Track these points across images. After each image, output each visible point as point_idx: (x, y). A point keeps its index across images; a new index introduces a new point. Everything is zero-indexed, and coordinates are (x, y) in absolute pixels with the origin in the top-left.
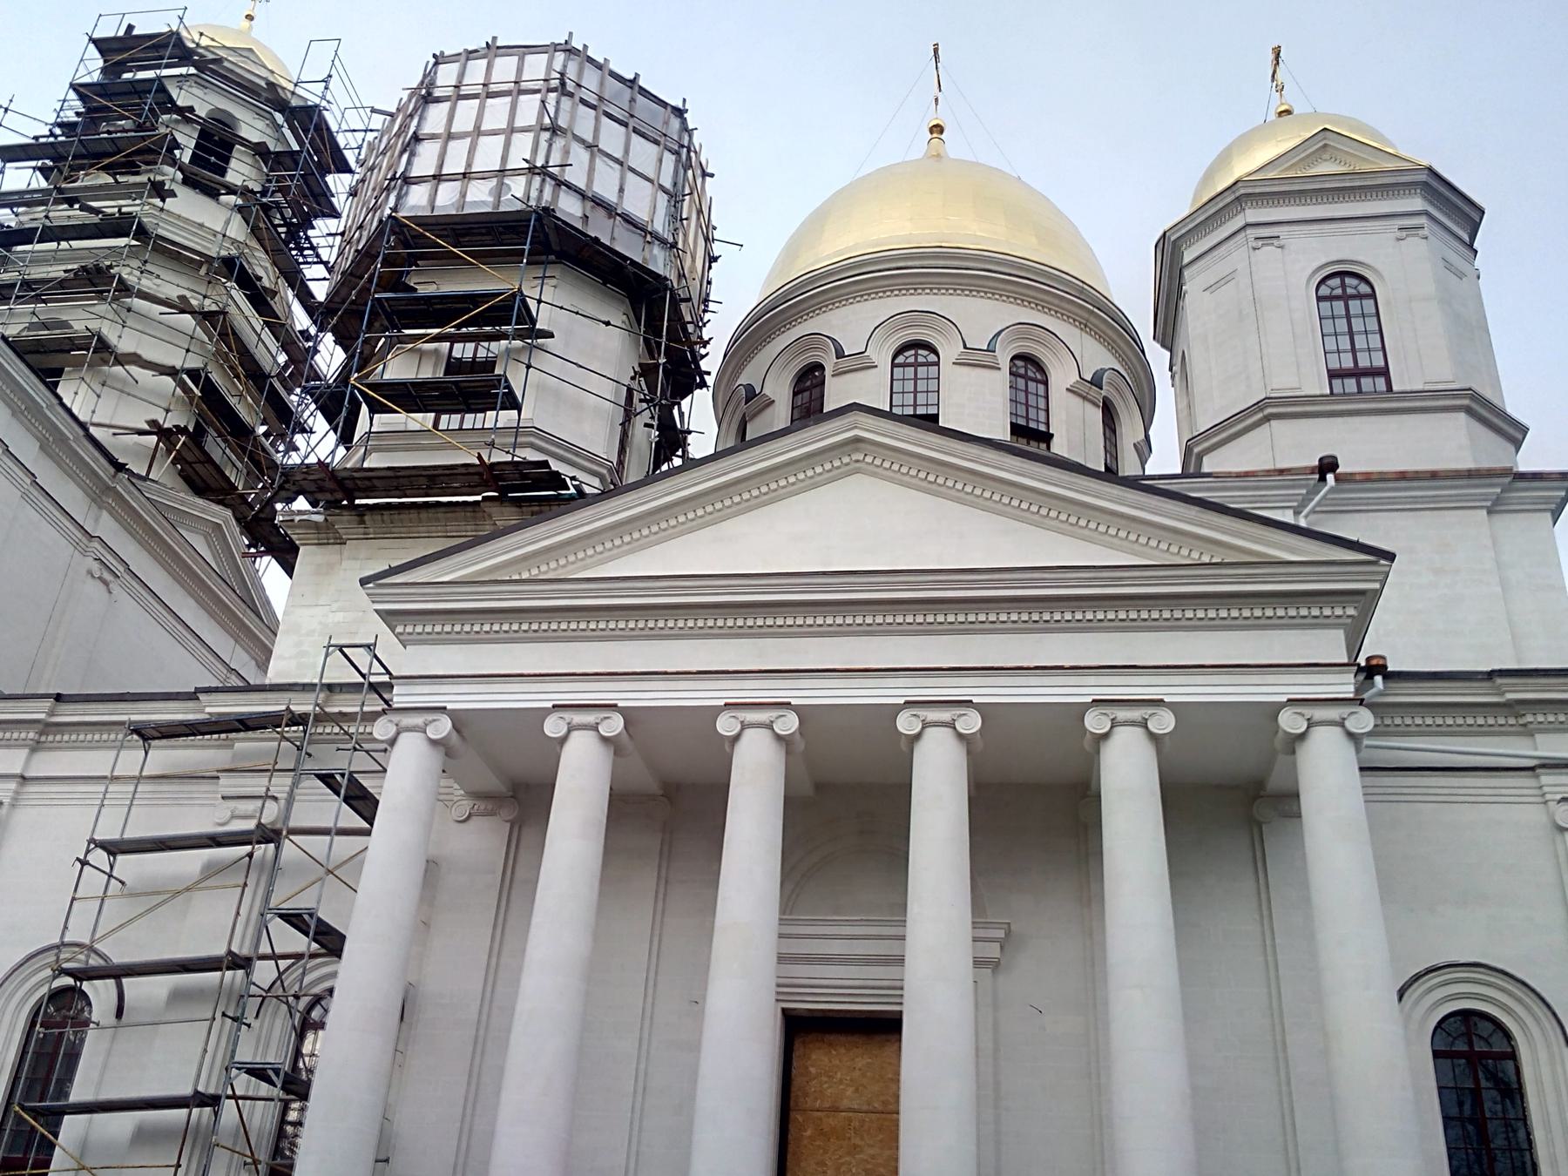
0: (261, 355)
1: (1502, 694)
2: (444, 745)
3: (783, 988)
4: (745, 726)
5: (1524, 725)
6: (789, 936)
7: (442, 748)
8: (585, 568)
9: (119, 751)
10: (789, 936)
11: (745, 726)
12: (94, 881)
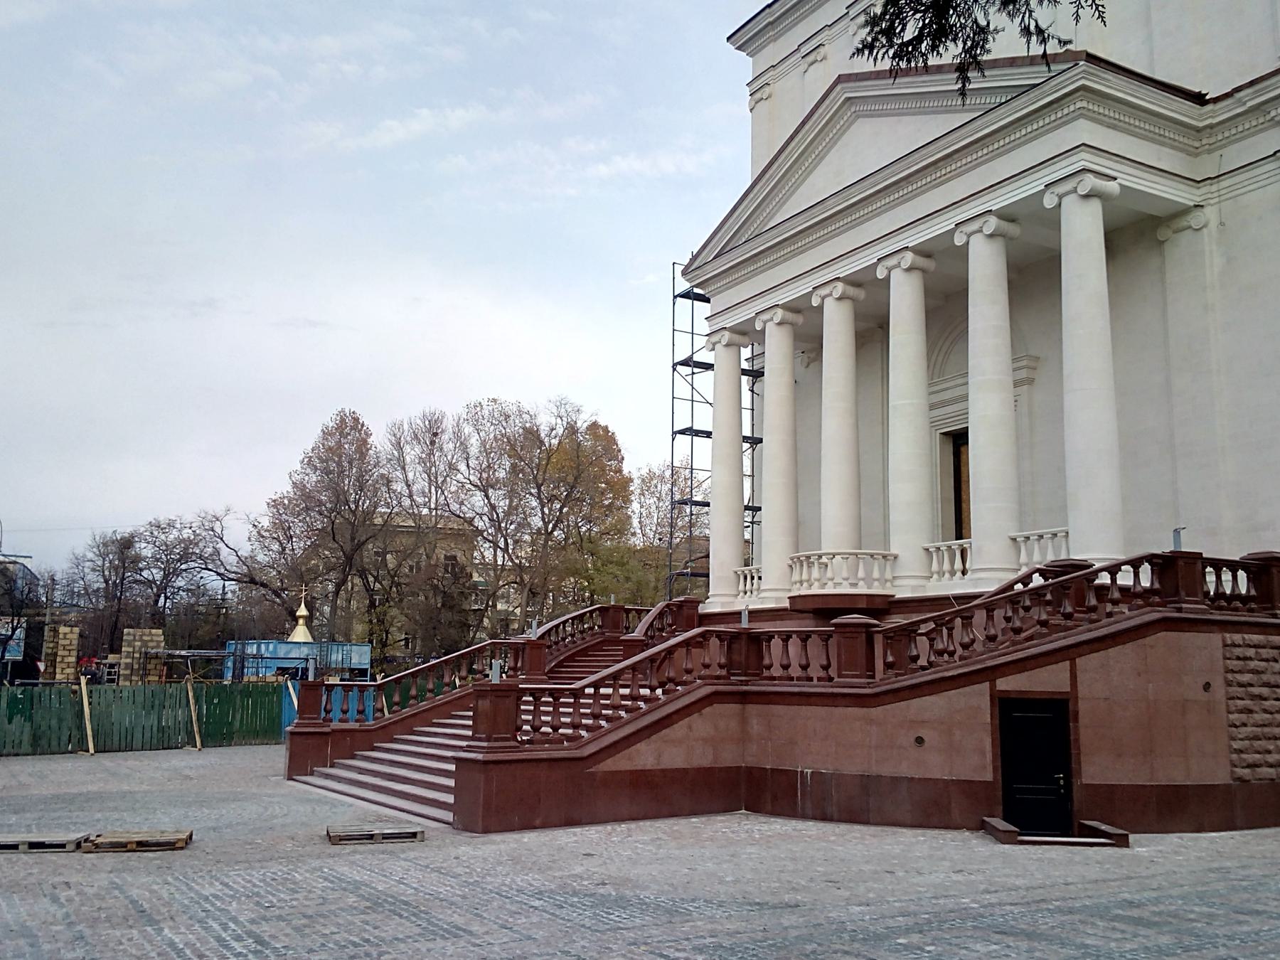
0: (744, 469)
1: (1245, 103)
2: (1000, 235)
3: (933, 423)
4: (1061, 197)
5: (1272, 119)
6: (943, 404)
7: (1000, 239)
8: (765, 226)
9: (1073, 661)
10: (943, 404)
11: (1061, 197)
12: (683, 390)
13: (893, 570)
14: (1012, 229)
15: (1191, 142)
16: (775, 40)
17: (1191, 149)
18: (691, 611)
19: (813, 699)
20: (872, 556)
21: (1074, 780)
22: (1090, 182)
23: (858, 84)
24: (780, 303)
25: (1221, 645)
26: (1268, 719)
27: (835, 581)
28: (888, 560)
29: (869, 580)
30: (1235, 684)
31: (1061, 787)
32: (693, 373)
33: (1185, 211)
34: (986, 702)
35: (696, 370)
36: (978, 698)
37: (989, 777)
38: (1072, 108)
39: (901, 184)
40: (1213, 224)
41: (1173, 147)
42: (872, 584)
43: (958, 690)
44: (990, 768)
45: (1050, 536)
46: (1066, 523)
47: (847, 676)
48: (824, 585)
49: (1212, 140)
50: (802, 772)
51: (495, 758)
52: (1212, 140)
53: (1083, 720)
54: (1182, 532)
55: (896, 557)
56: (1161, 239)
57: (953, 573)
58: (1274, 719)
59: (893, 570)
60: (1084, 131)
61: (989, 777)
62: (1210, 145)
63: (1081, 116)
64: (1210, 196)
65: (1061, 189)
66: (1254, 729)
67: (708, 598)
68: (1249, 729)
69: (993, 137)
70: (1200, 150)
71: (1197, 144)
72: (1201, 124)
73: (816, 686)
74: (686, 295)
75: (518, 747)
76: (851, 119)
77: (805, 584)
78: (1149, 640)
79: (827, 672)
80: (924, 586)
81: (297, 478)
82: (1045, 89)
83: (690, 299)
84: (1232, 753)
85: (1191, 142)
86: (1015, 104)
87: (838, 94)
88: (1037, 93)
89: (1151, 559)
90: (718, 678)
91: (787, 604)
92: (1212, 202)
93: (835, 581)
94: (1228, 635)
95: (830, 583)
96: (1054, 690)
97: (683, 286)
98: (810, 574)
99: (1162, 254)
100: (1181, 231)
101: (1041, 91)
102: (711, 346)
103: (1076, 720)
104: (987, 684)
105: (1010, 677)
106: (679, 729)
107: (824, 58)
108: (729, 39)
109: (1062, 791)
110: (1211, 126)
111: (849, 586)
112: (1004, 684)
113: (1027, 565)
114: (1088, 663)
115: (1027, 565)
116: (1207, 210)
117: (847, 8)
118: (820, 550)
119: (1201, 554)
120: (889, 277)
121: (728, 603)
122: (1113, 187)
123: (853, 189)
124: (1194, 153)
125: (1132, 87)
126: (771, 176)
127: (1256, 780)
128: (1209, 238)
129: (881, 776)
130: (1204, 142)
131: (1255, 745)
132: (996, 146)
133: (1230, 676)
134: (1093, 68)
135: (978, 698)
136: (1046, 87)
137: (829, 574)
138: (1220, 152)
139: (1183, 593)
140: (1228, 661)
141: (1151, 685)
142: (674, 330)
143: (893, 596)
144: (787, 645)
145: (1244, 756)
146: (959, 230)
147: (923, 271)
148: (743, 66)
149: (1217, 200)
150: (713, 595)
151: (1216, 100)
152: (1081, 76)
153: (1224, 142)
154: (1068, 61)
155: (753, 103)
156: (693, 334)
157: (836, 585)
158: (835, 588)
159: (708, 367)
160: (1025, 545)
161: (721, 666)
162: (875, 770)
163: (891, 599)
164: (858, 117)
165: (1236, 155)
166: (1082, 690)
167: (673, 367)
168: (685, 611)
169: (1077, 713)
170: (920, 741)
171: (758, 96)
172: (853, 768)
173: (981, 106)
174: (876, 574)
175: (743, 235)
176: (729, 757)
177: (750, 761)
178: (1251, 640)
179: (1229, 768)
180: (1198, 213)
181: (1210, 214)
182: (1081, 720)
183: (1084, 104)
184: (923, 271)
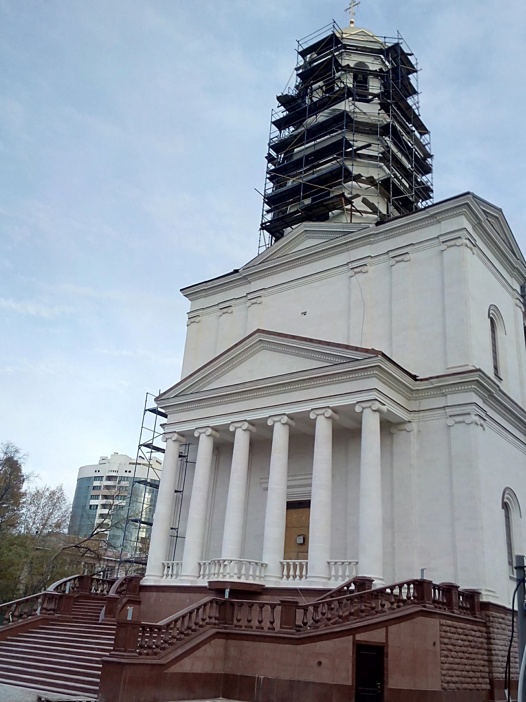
2: (331, 418)
4: (363, 408)
11: (363, 408)
13: (265, 572)
14: (336, 417)
15: (409, 395)
16: (205, 297)
17: (408, 397)
18: (136, 583)
19: (267, 639)
20: (250, 563)
21: (385, 686)
22: (377, 405)
23: (268, 335)
24: (211, 425)
25: (439, 625)
26: (453, 660)
27: (230, 575)
28: (258, 565)
29: (247, 577)
30: (443, 643)
31: (379, 689)
32: (152, 452)
33: (404, 422)
34: (350, 646)
35: (153, 451)
36: (347, 643)
37: (350, 683)
38: (372, 373)
39: (285, 385)
40: (415, 430)
41: (403, 396)
42: (248, 578)
43: (339, 639)
44: (351, 679)
45: (334, 563)
46: (358, 558)
47: (285, 628)
48: (224, 576)
49: (417, 396)
50: (258, 678)
51: (138, 662)
52: (417, 396)
53: (390, 657)
54: (424, 570)
55: (267, 565)
56: (392, 432)
57: (288, 577)
58: (455, 661)
59: (265, 572)
60: (374, 383)
61: (350, 683)
62: (416, 397)
63: (375, 377)
64: (415, 418)
65: (364, 405)
66: (449, 665)
67: (145, 576)
68: (447, 665)
69: (334, 376)
70: (411, 398)
71: (411, 396)
72: (414, 388)
73: (244, 630)
74: (153, 411)
75: (138, 656)
76: (260, 349)
77: (216, 575)
78: (415, 620)
79: (273, 625)
80: (279, 582)
81: (28, 492)
82: (362, 362)
83: (155, 413)
84: (442, 676)
85: (409, 395)
86: (347, 365)
87: (256, 337)
88: (358, 363)
89: (414, 582)
90: (215, 624)
91: (207, 584)
92: (415, 421)
93: (230, 575)
94: (441, 620)
95: (228, 576)
96: (378, 641)
97: (153, 405)
98: (219, 570)
99: (392, 439)
100: (401, 431)
101: (360, 363)
102: (165, 440)
103: (387, 657)
104: (351, 636)
105: (362, 634)
106: (199, 653)
107: (232, 312)
108: (181, 290)
109: (379, 691)
110: (417, 390)
111: (237, 577)
112: (360, 637)
113: (349, 576)
114: (392, 629)
115: (349, 576)
116: (413, 424)
117: (247, 294)
118: (221, 558)
119: (432, 581)
120: (273, 425)
121: (157, 580)
122: (384, 408)
123: (261, 382)
124: (409, 399)
125: (394, 369)
126: (215, 365)
127: (449, 689)
128: (413, 436)
129: (300, 681)
130: (414, 395)
131: (449, 673)
132: (334, 379)
133: (442, 639)
134: (384, 359)
135: (347, 643)
136: (362, 362)
137: (228, 571)
138: (420, 401)
139: (426, 599)
140: (441, 632)
141: (415, 642)
142: (142, 427)
143: (264, 586)
144: (273, 611)
145: (446, 678)
146: (313, 412)
147: (290, 426)
148: (186, 304)
149: (418, 420)
150: (148, 575)
151: (421, 380)
152: (378, 361)
153: (422, 397)
154: (373, 354)
155: (189, 323)
156: (154, 432)
157: (231, 577)
158: (230, 578)
159: (163, 451)
160: (335, 567)
161: (216, 618)
162: (296, 678)
163: (264, 587)
164: (264, 349)
165: (426, 404)
166: (390, 642)
167: (139, 446)
168: (134, 583)
169: (387, 653)
170: (320, 663)
171: (192, 320)
172: (286, 676)
173: (333, 362)
174: (258, 574)
175: (191, 390)
176: (219, 669)
177: (228, 671)
178: (448, 623)
179: (441, 683)
180: (409, 424)
181: (414, 426)
182: (389, 657)
183: (377, 372)
184: (290, 426)
